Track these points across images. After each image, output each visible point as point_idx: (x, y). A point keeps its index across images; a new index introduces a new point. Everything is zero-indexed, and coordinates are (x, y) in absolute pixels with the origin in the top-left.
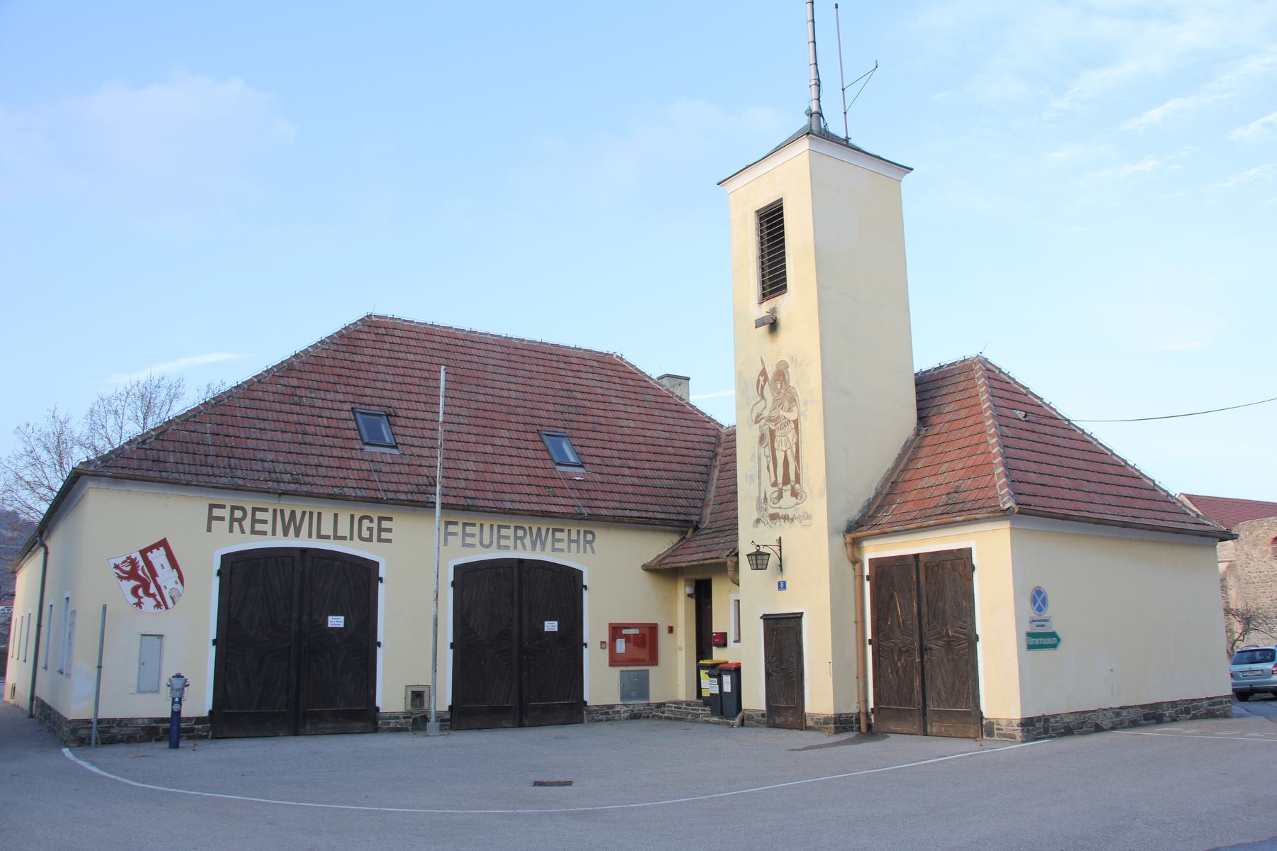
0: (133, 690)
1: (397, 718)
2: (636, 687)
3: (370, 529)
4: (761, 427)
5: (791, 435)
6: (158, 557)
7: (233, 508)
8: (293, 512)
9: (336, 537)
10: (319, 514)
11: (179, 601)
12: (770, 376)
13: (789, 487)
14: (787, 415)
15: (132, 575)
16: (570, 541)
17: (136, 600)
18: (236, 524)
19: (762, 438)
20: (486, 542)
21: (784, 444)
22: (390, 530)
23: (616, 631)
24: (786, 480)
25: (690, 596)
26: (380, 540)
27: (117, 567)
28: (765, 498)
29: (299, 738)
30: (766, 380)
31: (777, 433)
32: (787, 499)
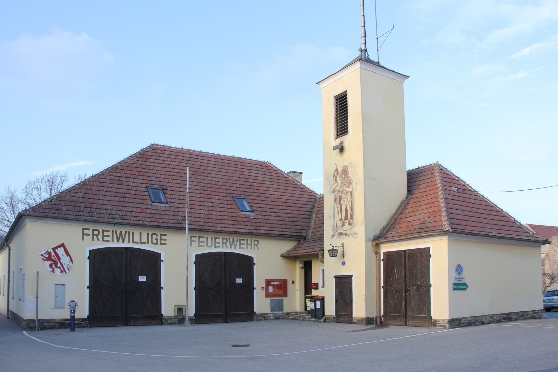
3: (156, 239)
5: (349, 198)
6: (61, 251)
8: (121, 232)
9: (141, 243)
10: (133, 233)
13: (347, 221)
14: (347, 189)
15: (49, 259)
16: (248, 244)
17: (52, 270)
18: (95, 237)
19: (335, 200)
21: (345, 202)
23: (268, 282)
24: (346, 218)
25: (302, 268)
26: (161, 244)
27: (42, 255)
28: (337, 226)
29: (128, 327)
30: (338, 173)
31: (343, 197)
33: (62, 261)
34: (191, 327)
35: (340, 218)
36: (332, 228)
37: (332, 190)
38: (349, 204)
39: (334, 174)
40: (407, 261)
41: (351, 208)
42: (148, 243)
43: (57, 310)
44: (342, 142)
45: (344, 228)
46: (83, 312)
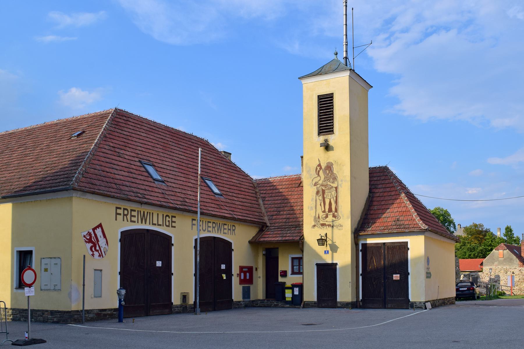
0: (93, 296)
1: (178, 307)
2: (246, 293)
3: (169, 221)
4: (317, 188)
5: (334, 193)
6: (99, 232)
7: (124, 209)
8: (144, 212)
9: (159, 225)
10: (153, 213)
11: (107, 253)
12: (323, 167)
13: (332, 213)
14: (332, 184)
15: (90, 241)
16: (229, 229)
17: (92, 253)
18: (125, 217)
19: (318, 193)
20: (204, 229)
21: (329, 196)
22: (175, 222)
23: (241, 268)
24: (330, 210)
25: (264, 255)
26: (172, 227)
27: (84, 236)
28: (319, 217)
29: (149, 318)
30: (321, 168)
31: (326, 191)
32: (330, 218)
33: (100, 243)
34: (201, 315)
35: (323, 209)
36: (313, 219)
37: (314, 183)
38: (333, 198)
39: (317, 169)
40: (386, 252)
41: (336, 202)
42: (138, 222)
43: (96, 299)
44: (326, 141)
45: (327, 219)
46: (111, 299)
